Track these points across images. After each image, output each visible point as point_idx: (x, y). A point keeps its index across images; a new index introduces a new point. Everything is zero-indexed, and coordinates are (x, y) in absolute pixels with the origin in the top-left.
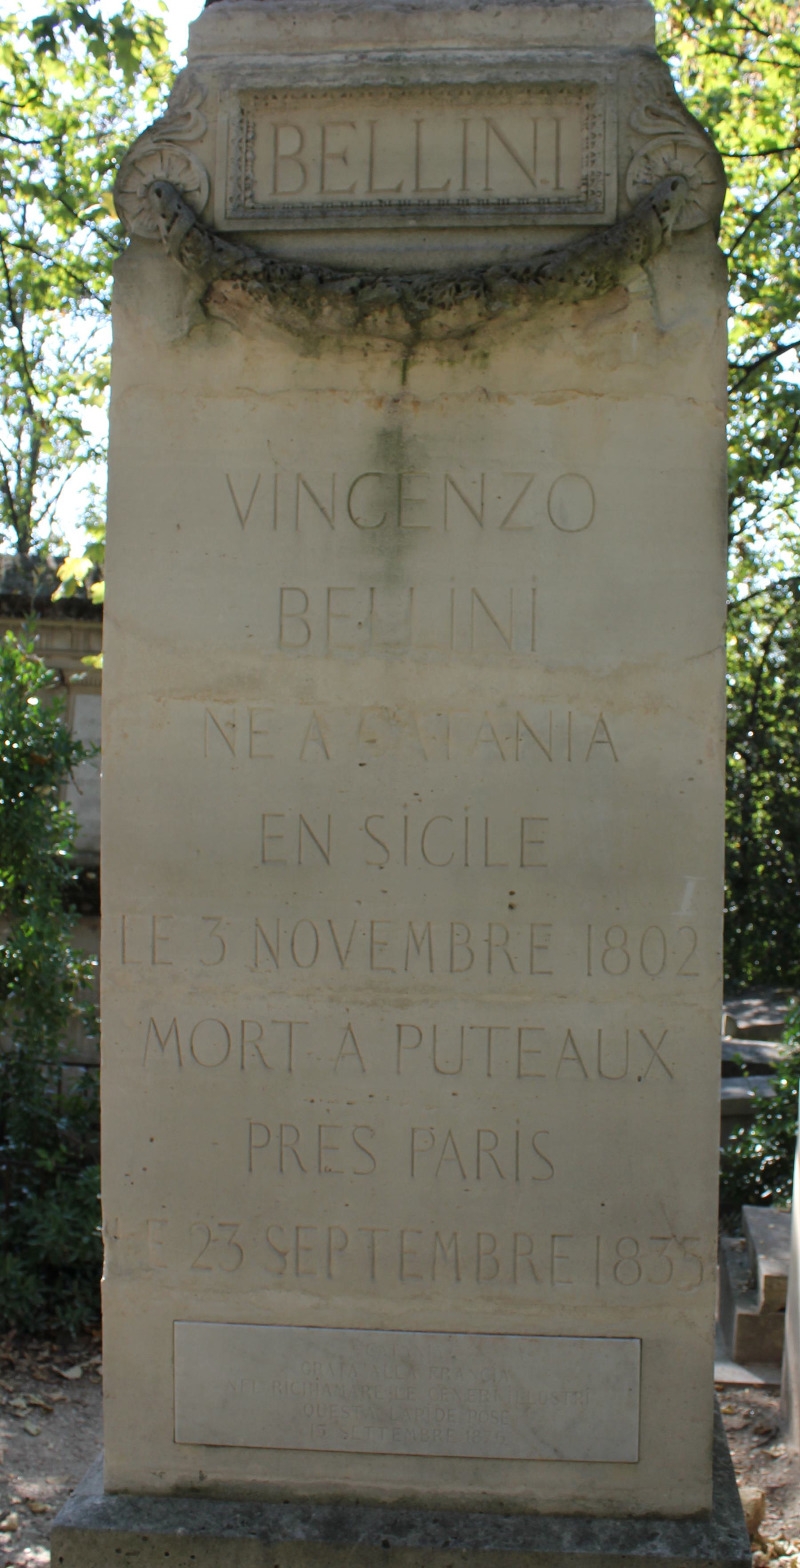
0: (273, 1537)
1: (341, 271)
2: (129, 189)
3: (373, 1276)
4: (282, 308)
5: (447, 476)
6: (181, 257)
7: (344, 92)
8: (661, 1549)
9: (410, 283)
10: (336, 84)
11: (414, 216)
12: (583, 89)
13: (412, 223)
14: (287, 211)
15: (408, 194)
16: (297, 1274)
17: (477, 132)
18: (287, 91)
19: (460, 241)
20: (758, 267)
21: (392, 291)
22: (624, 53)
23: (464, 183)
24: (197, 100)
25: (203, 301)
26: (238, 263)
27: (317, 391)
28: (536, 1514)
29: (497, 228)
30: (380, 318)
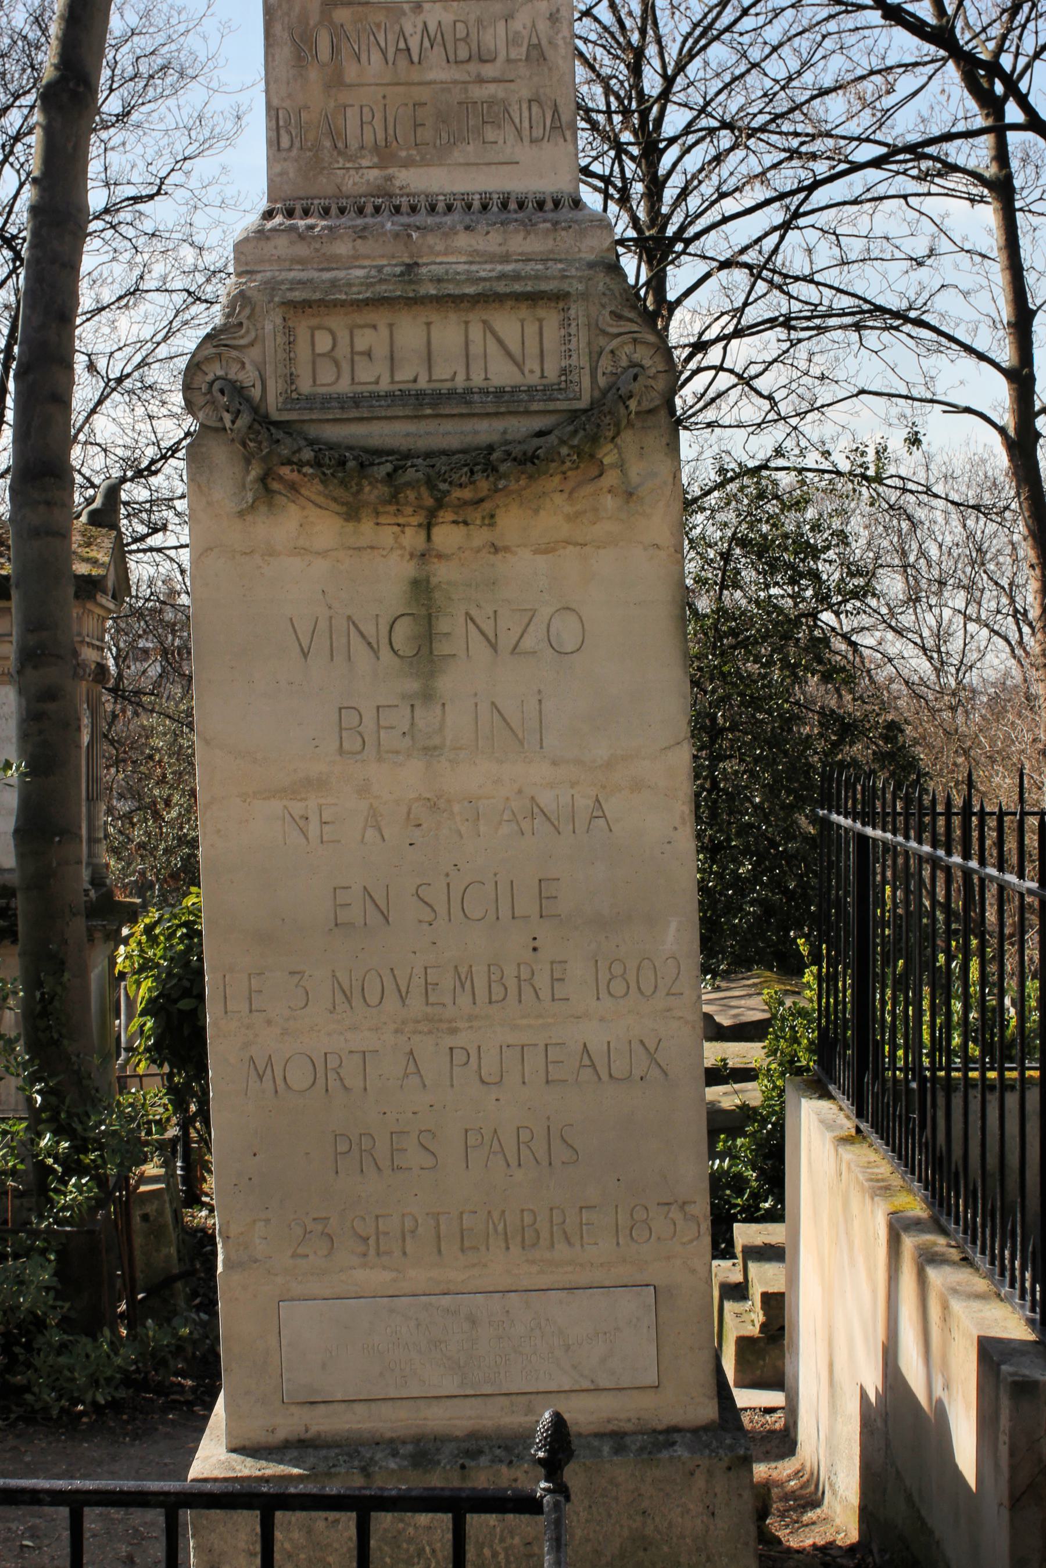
0: (371, 1469)
2: (195, 386)
3: (440, 1251)
4: (331, 488)
5: (467, 614)
6: (244, 445)
7: (367, 302)
9: (433, 466)
10: (361, 297)
11: (433, 405)
12: (559, 298)
13: (429, 411)
14: (326, 401)
15: (423, 384)
16: (378, 1254)
17: (476, 332)
18: (321, 303)
19: (469, 425)
21: (420, 475)
22: (591, 265)
23: (468, 374)
24: (247, 311)
26: (294, 453)
27: (359, 549)
29: (497, 414)
30: (411, 495)
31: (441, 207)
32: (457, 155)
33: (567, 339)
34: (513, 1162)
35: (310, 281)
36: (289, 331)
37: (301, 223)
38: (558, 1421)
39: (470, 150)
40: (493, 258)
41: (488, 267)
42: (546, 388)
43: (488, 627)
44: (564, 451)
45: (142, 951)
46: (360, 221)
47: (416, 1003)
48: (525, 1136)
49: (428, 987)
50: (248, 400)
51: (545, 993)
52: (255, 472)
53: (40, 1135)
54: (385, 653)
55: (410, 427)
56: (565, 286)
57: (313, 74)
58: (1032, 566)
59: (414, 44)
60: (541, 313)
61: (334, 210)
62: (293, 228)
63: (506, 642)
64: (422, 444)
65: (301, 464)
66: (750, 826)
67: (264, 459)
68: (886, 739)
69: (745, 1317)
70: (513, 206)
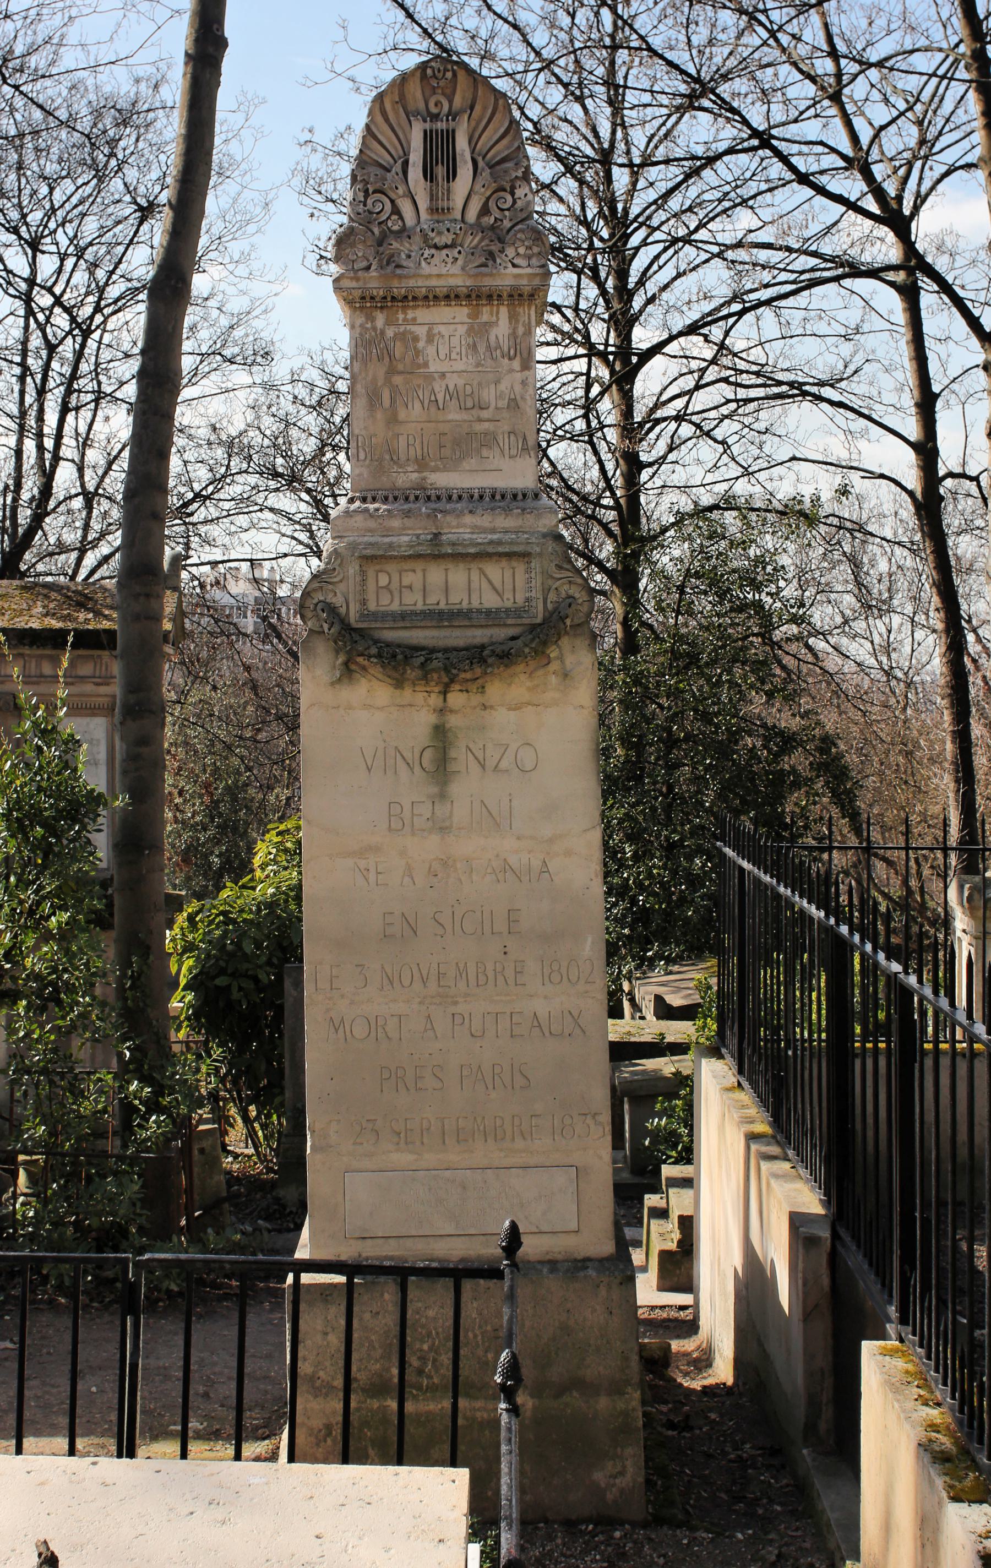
6: (336, 643)
7: (410, 557)
11: (449, 620)
12: (525, 556)
15: (442, 606)
17: (475, 576)
18: (382, 557)
19: (470, 633)
22: (545, 536)
24: (339, 561)
28: (529, 1262)
29: (487, 626)
30: (435, 676)
31: (455, 497)
32: (465, 465)
33: (529, 580)
34: (491, 1087)
35: (376, 543)
36: (363, 573)
37: (372, 507)
38: (514, 1226)
39: (472, 463)
40: (485, 531)
41: (483, 536)
42: (517, 610)
43: (480, 755)
44: (527, 650)
45: (183, 934)
46: (406, 507)
47: (433, 984)
48: (497, 1070)
49: (440, 975)
50: (338, 615)
51: (511, 981)
52: (341, 659)
53: (129, 1082)
54: (417, 768)
55: (434, 633)
56: (529, 549)
57: (379, 415)
58: (937, 610)
59: (440, 397)
60: (514, 564)
61: (391, 498)
62: (367, 510)
63: (490, 764)
64: (441, 644)
65: (370, 656)
66: (702, 827)
67: (348, 652)
68: (822, 751)
69: (667, 1236)
70: (498, 497)
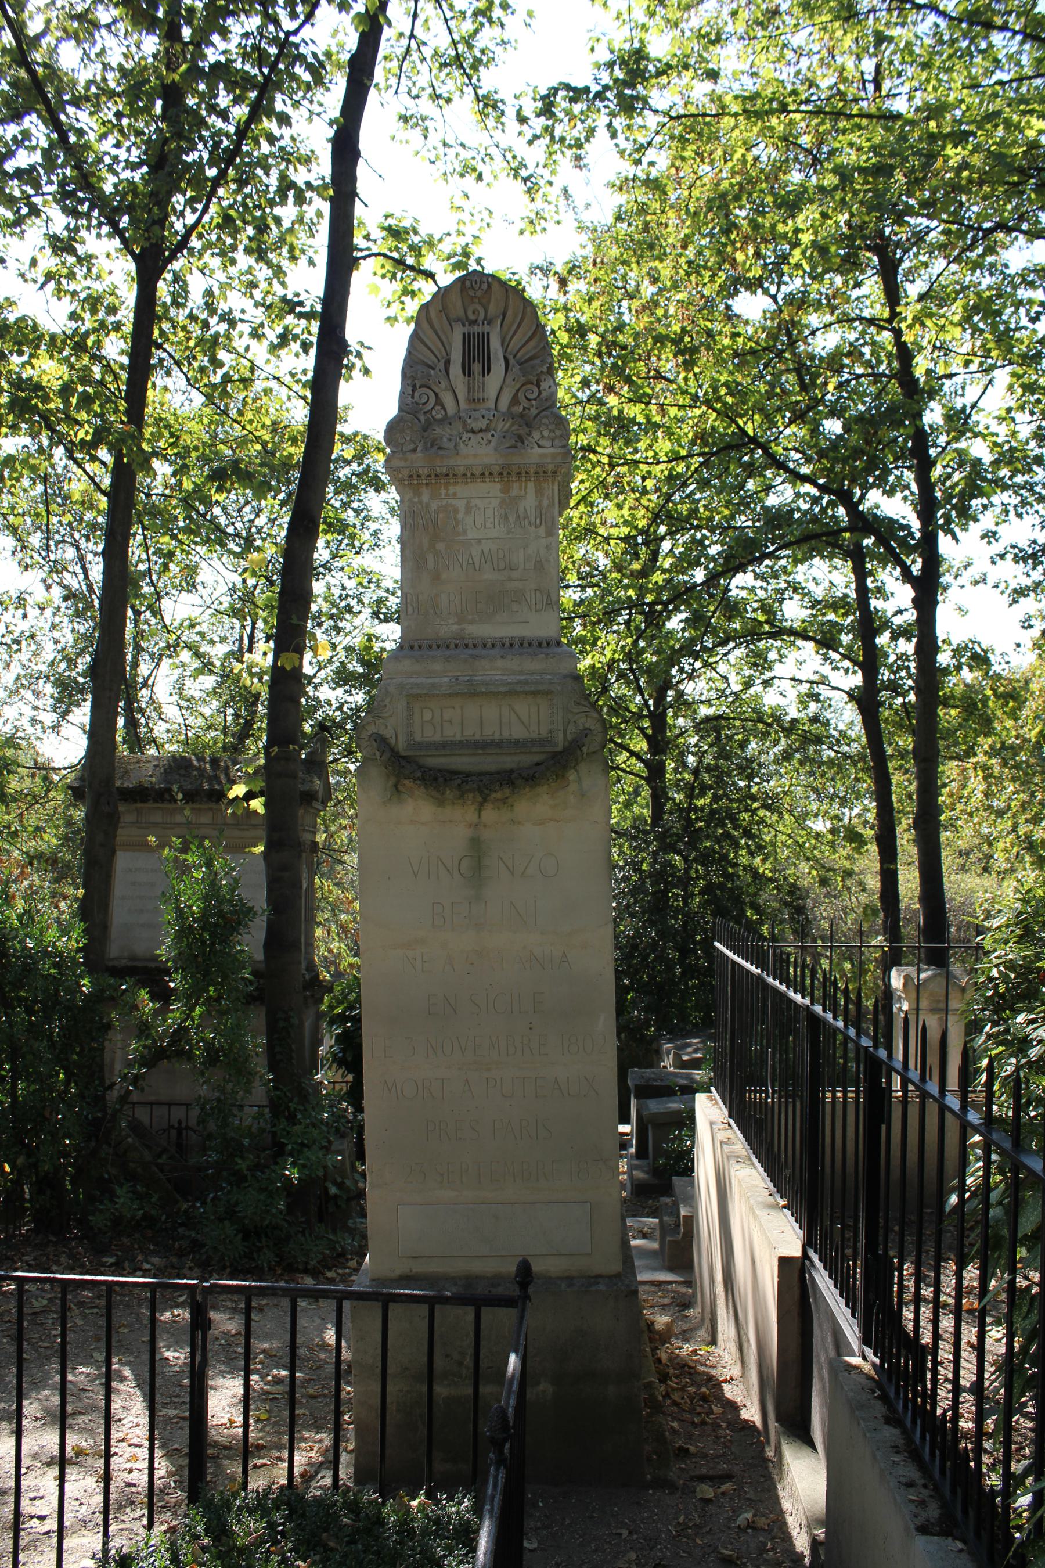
1: (454, 773)
7: (450, 695)
8: (602, 1287)
12: (548, 693)
15: (477, 737)
20: (771, 101)
25: (396, 786)
30: (471, 795)
